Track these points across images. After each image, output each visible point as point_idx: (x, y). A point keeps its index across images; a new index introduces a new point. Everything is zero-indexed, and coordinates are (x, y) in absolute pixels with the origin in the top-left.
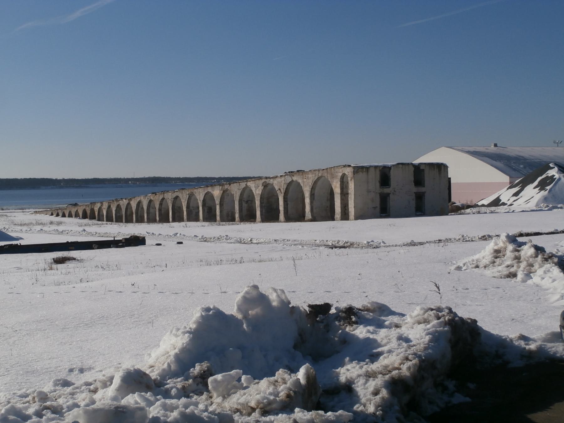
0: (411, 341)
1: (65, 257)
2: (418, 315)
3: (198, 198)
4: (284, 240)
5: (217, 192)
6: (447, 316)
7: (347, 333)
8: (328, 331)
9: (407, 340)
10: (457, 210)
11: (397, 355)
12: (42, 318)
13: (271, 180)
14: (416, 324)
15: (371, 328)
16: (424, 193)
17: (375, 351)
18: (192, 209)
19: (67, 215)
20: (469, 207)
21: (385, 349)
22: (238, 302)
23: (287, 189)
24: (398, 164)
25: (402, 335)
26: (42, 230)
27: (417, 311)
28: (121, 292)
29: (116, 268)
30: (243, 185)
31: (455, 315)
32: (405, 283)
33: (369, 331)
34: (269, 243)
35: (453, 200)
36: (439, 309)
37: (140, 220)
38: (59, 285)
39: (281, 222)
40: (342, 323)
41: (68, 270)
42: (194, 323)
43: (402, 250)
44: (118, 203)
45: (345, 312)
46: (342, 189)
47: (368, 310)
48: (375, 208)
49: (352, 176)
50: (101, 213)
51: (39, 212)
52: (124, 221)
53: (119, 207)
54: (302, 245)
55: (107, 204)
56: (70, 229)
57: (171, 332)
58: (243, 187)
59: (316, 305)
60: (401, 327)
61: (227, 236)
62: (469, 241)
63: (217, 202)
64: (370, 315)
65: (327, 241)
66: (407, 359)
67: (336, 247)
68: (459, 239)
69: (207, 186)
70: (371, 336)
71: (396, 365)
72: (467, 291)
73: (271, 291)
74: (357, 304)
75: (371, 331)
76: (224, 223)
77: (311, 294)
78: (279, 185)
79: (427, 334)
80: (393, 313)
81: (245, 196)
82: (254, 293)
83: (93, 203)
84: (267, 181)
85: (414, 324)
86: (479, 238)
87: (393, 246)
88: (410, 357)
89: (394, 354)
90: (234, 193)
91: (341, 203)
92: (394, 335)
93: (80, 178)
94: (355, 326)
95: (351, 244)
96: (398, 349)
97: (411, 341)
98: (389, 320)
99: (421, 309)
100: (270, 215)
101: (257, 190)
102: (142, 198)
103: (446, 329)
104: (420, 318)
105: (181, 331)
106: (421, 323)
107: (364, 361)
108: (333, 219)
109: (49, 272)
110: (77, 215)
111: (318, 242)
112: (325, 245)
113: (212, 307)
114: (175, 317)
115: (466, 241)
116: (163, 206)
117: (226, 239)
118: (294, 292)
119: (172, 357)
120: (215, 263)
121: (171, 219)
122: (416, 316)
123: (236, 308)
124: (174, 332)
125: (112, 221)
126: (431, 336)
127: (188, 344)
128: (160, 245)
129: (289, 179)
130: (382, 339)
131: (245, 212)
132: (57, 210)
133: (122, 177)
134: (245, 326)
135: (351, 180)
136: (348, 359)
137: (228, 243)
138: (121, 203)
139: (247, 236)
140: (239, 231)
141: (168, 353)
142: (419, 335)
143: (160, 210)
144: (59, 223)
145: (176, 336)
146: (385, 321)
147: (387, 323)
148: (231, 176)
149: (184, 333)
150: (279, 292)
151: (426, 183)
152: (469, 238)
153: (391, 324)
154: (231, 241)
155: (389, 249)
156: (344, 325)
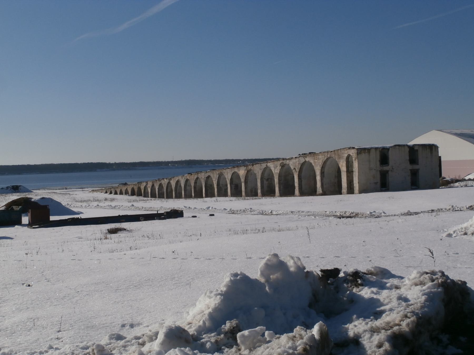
0: (410, 301)
1: (117, 228)
2: (415, 278)
3: (226, 177)
4: (299, 212)
5: (242, 172)
6: (440, 279)
7: (354, 294)
8: (338, 292)
9: (406, 300)
10: (447, 184)
11: (398, 313)
12: (99, 281)
13: (288, 161)
14: (414, 286)
15: (374, 290)
16: (418, 170)
17: (378, 309)
19: (118, 193)
20: (457, 181)
21: (387, 307)
22: (261, 268)
23: (300, 168)
24: (395, 146)
25: (402, 295)
26: (98, 205)
27: (414, 274)
28: (163, 258)
29: (160, 238)
30: (264, 165)
31: (447, 277)
33: (373, 292)
34: (287, 214)
35: (443, 175)
36: (433, 273)
37: (179, 196)
38: (113, 252)
39: (296, 196)
40: (349, 285)
41: (120, 239)
42: (225, 286)
43: (401, 220)
47: (371, 273)
48: (376, 183)
50: (146, 191)
51: (95, 190)
52: (165, 197)
53: (161, 185)
54: (315, 215)
55: (151, 184)
56: (121, 204)
57: (206, 294)
59: (327, 270)
61: (251, 209)
62: (458, 210)
65: (336, 212)
66: (406, 316)
67: (343, 217)
68: (449, 209)
69: (234, 167)
70: (375, 297)
71: (397, 322)
72: (457, 255)
73: (288, 258)
74: (363, 268)
76: (248, 198)
77: (322, 259)
78: (294, 165)
79: (423, 295)
80: (394, 276)
81: (266, 175)
82: (275, 260)
83: (140, 183)
84: (284, 162)
85: (412, 286)
86: (467, 208)
87: (392, 215)
88: (409, 315)
89: (395, 312)
91: (347, 180)
92: (394, 295)
93: (129, 162)
94: (361, 287)
96: (398, 307)
97: (410, 301)
98: (390, 282)
99: (418, 273)
100: (288, 191)
101: (276, 170)
102: (180, 178)
103: (439, 290)
104: (417, 280)
105: (214, 293)
106: (417, 285)
107: (369, 318)
108: (340, 193)
109: (105, 241)
110: (127, 193)
111: (328, 212)
112: (334, 216)
113: (239, 273)
114: (209, 279)
115: (456, 211)
116: (198, 184)
118: (308, 257)
119: (206, 316)
120: (241, 232)
121: (204, 195)
122: (413, 279)
123: (259, 273)
124: (208, 294)
125: (155, 197)
126: (426, 296)
128: (195, 217)
129: (302, 160)
130: (385, 299)
131: (266, 188)
133: (163, 161)
134: (267, 289)
135: (355, 160)
136: (355, 316)
138: (163, 182)
139: (267, 208)
140: (261, 204)
141: (203, 312)
142: (416, 295)
143: (195, 188)
144: (112, 200)
145: (210, 297)
146: (386, 283)
147: (388, 285)
149: (216, 295)
150: (296, 259)
151: (420, 161)
152: (458, 208)
153: (391, 286)
154: (254, 213)
155: (388, 218)
156: (351, 287)
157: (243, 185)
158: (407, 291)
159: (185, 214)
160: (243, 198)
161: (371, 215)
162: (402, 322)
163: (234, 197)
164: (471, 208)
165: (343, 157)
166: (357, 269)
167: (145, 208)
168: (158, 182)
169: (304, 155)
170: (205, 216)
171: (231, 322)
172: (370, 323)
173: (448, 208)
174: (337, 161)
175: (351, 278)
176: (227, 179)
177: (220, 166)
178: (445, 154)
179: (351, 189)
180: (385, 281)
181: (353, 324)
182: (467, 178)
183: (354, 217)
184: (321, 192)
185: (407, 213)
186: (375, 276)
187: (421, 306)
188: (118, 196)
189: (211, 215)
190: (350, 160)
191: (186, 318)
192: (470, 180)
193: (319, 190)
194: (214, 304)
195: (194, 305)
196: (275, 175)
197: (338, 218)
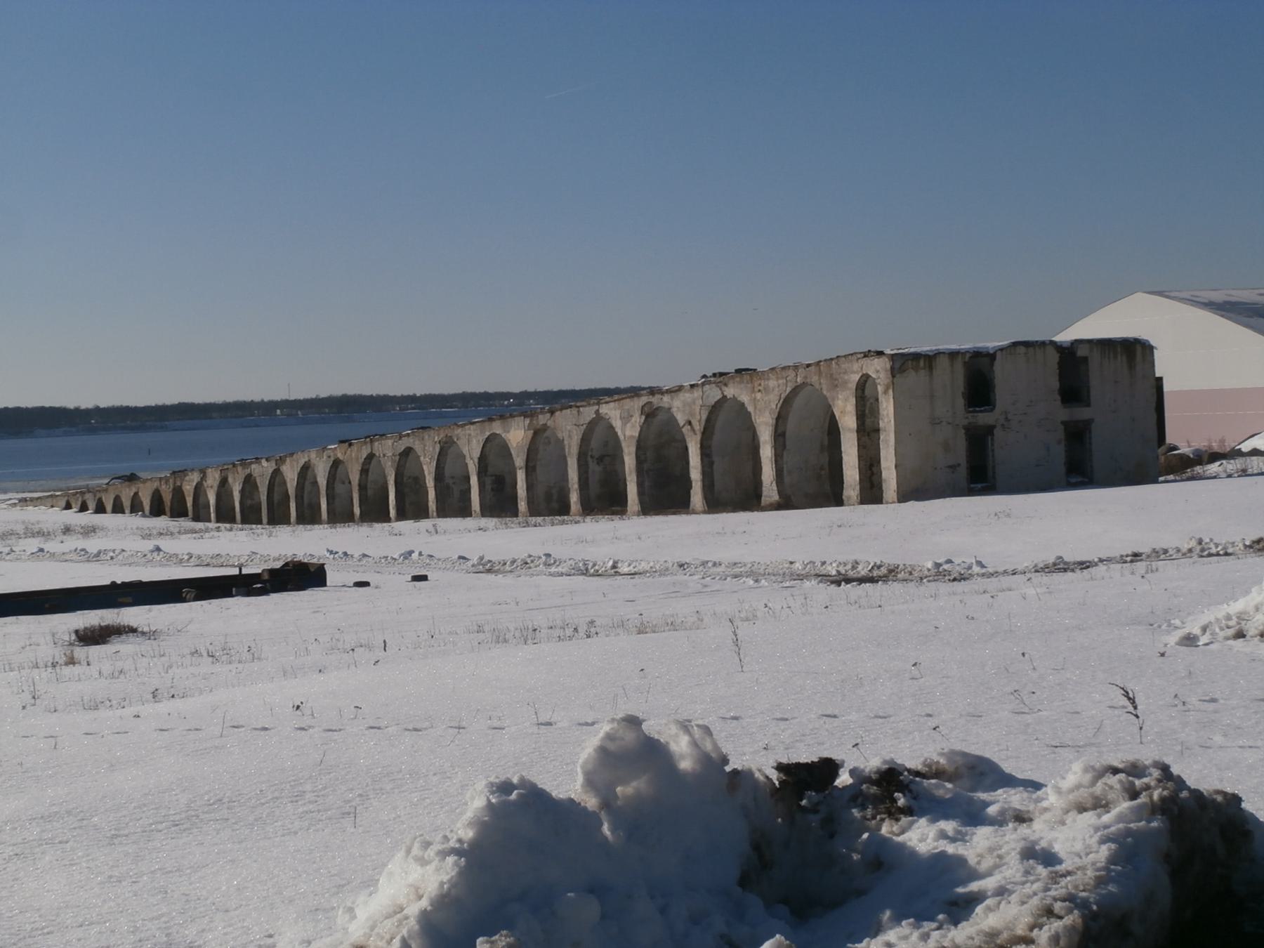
0: (1060, 862)
1: (107, 627)
2: (1078, 787)
3: (465, 451)
4: (704, 563)
5: (516, 435)
6: (1156, 788)
7: (885, 841)
8: (832, 836)
9: (1049, 859)
10: (1184, 466)
11: (1023, 903)
12: (55, 809)
13: (666, 398)
14: (1073, 814)
15: (949, 826)
16: (1087, 424)
17: (960, 890)
18: (451, 481)
19: (109, 507)
20: (1215, 457)
21: (989, 884)
22: (586, 762)
23: (708, 420)
24: (1015, 344)
25: (1035, 843)
26: (41, 550)
27: (1075, 775)
28: (266, 729)
29: (249, 657)
30: (588, 413)
31: (1180, 783)
32: (1043, 670)
33: (943, 835)
34: (664, 572)
35: (1170, 438)
36: (1135, 770)
37: (309, 516)
38: (96, 708)
39: (694, 512)
40: (869, 812)
41: (119, 665)
42: (470, 824)
44: (248, 471)
45: (876, 783)
46: (861, 416)
47: (939, 774)
48: (953, 468)
49: (889, 381)
50: (201, 500)
51: (32, 500)
52: (265, 520)
53: (249, 482)
55: (217, 475)
56: (118, 545)
57: (408, 851)
58: (588, 419)
59: (798, 766)
60: (1031, 820)
61: (548, 555)
62: (1218, 554)
63: (519, 461)
64: (946, 789)
65: (823, 563)
66: (1049, 912)
67: (848, 581)
68: (1190, 550)
69: (491, 420)
70: (951, 849)
71: (1020, 931)
72: (1212, 706)
73: (674, 729)
74: (911, 757)
75: (950, 834)
76: (539, 519)
77: (782, 725)
78: (687, 411)
79: (1103, 841)
80: (1008, 781)
82: (629, 737)
83: (180, 473)
84: (655, 400)
86: (1246, 546)
87: (1005, 572)
88: (1058, 907)
89: (1014, 898)
90: (565, 435)
91: (859, 457)
92: (1013, 845)
93: (141, 404)
94: (905, 820)
95: (890, 571)
96: (1024, 883)
97: (1060, 862)
98: (1000, 800)
99: (1086, 770)
100: (666, 495)
101: (627, 425)
102: (313, 455)
103: (1155, 824)
104: (1083, 794)
105: (437, 847)
106: (1085, 810)
107: (932, 919)
108: (837, 499)
109: (68, 671)
110: (136, 507)
111: (798, 566)
112: (817, 575)
113: (515, 780)
115: (1210, 555)
116: (371, 477)
117: (547, 565)
119: (413, 923)
122: (1071, 791)
123: (580, 779)
124: (416, 850)
125: (232, 520)
126: (1113, 846)
127: (453, 885)
128: (366, 584)
129: (714, 394)
130: (981, 856)
131: (594, 488)
132: (82, 493)
133: (257, 398)
134: (606, 829)
135: (886, 392)
136: (888, 913)
137: (551, 575)
139: (601, 554)
140: (581, 541)
141: (402, 909)
142: (1082, 843)
143: (362, 487)
144: (89, 531)
145: (423, 862)
146: (987, 804)
147: (992, 810)
148: (555, 386)
149: (443, 854)
150: (697, 733)
151: (1095, 393)
152: (1217, 545)
153: (1002, 812)
154: (560, 569)
155: (992, 584)
156: (874, 818)
157: (521, 477)
158: (1052, 829)
159: (331, 577)
160: (520, 519)
161: (938, 574)
162: (1036, 931)
163: (492, 516)
164: (1263, 546)
165: (846, 382)
166: (892, 761)
167: (199, 557)
168: (240, 469)
169: (721, 377)
170: (394, 582)
171: (492, 943)
172: (936, 935)
173: (1185, 547)
174: (825, 398)
175: (874, 790)
176: (468, 461)
177: (442, 416)
178: (1170, 367)
179: (872, 486)
180: (983, 796)
181: (881, 939)
182: (1246, 447)
183: (884, 579)
184: (776, 497)
185: (1055, 564)
186: (949, 781)
187: (1097, 878)
188: (107, 519)
189: (417, 578)
190: (867, 392)
191: (345, 929)
192: (1255, 452)
193: (770, 491)
194: (436, 885)
195: (370, 884)
196: (624, 445)
197: (832, 582)
